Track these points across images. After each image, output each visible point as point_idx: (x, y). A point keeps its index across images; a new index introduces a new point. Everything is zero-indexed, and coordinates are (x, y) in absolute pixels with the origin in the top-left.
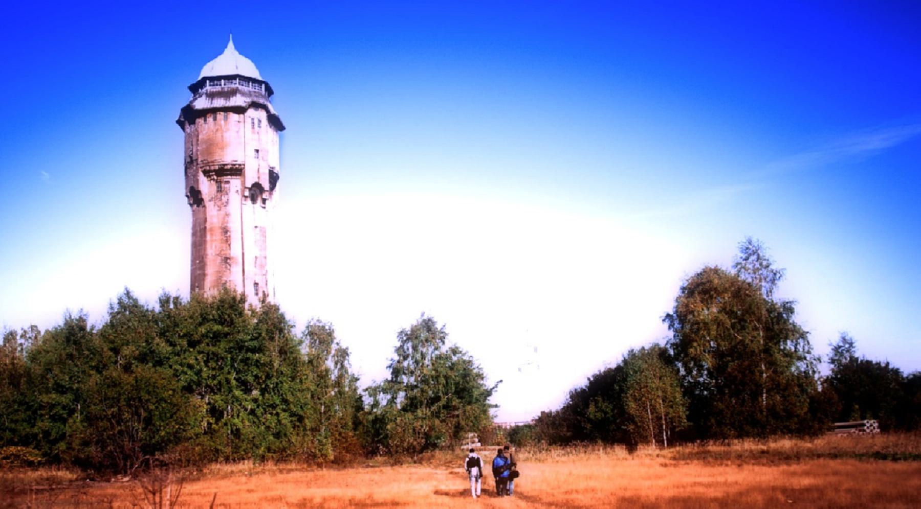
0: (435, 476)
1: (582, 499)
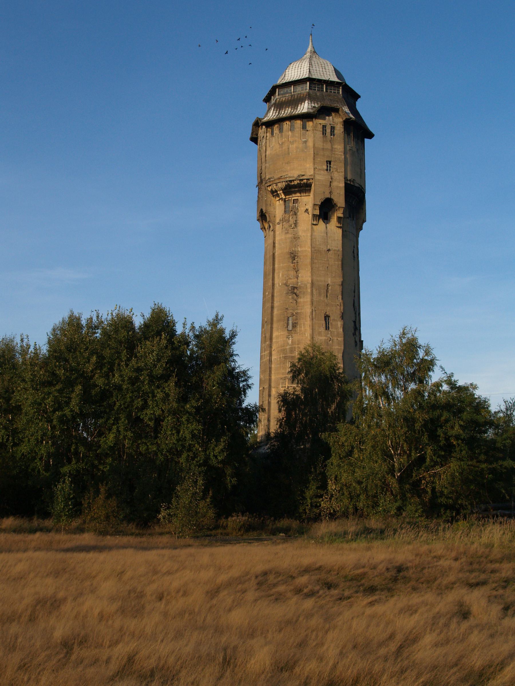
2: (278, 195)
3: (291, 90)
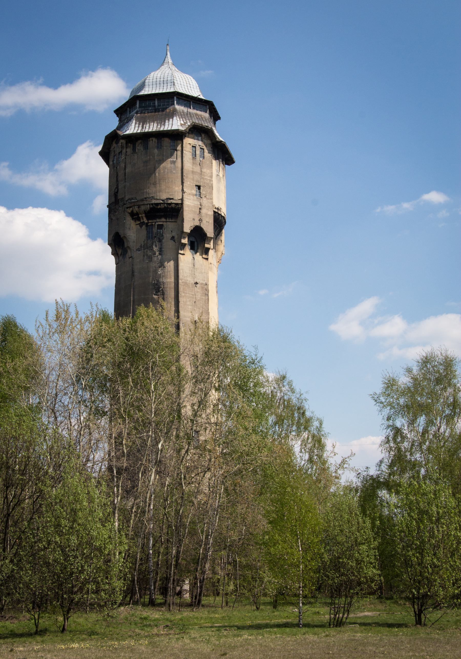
0: (340, 620)
1: (69, 84)
2: (138, 219)
3: (155, 103)
